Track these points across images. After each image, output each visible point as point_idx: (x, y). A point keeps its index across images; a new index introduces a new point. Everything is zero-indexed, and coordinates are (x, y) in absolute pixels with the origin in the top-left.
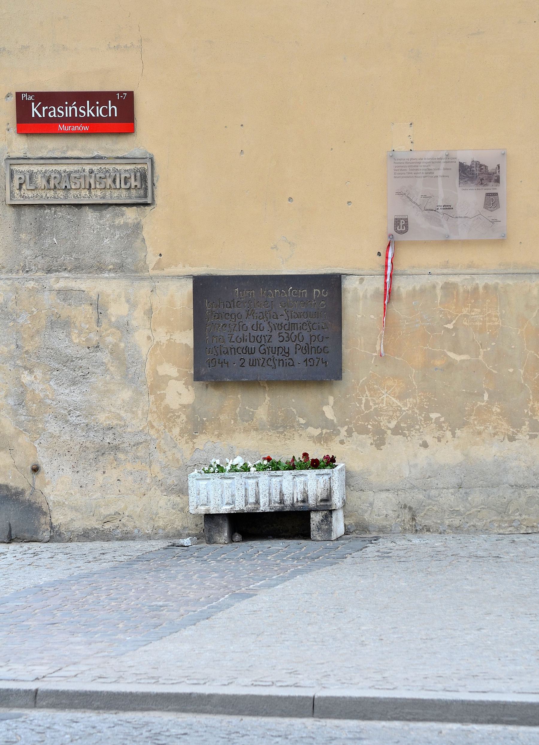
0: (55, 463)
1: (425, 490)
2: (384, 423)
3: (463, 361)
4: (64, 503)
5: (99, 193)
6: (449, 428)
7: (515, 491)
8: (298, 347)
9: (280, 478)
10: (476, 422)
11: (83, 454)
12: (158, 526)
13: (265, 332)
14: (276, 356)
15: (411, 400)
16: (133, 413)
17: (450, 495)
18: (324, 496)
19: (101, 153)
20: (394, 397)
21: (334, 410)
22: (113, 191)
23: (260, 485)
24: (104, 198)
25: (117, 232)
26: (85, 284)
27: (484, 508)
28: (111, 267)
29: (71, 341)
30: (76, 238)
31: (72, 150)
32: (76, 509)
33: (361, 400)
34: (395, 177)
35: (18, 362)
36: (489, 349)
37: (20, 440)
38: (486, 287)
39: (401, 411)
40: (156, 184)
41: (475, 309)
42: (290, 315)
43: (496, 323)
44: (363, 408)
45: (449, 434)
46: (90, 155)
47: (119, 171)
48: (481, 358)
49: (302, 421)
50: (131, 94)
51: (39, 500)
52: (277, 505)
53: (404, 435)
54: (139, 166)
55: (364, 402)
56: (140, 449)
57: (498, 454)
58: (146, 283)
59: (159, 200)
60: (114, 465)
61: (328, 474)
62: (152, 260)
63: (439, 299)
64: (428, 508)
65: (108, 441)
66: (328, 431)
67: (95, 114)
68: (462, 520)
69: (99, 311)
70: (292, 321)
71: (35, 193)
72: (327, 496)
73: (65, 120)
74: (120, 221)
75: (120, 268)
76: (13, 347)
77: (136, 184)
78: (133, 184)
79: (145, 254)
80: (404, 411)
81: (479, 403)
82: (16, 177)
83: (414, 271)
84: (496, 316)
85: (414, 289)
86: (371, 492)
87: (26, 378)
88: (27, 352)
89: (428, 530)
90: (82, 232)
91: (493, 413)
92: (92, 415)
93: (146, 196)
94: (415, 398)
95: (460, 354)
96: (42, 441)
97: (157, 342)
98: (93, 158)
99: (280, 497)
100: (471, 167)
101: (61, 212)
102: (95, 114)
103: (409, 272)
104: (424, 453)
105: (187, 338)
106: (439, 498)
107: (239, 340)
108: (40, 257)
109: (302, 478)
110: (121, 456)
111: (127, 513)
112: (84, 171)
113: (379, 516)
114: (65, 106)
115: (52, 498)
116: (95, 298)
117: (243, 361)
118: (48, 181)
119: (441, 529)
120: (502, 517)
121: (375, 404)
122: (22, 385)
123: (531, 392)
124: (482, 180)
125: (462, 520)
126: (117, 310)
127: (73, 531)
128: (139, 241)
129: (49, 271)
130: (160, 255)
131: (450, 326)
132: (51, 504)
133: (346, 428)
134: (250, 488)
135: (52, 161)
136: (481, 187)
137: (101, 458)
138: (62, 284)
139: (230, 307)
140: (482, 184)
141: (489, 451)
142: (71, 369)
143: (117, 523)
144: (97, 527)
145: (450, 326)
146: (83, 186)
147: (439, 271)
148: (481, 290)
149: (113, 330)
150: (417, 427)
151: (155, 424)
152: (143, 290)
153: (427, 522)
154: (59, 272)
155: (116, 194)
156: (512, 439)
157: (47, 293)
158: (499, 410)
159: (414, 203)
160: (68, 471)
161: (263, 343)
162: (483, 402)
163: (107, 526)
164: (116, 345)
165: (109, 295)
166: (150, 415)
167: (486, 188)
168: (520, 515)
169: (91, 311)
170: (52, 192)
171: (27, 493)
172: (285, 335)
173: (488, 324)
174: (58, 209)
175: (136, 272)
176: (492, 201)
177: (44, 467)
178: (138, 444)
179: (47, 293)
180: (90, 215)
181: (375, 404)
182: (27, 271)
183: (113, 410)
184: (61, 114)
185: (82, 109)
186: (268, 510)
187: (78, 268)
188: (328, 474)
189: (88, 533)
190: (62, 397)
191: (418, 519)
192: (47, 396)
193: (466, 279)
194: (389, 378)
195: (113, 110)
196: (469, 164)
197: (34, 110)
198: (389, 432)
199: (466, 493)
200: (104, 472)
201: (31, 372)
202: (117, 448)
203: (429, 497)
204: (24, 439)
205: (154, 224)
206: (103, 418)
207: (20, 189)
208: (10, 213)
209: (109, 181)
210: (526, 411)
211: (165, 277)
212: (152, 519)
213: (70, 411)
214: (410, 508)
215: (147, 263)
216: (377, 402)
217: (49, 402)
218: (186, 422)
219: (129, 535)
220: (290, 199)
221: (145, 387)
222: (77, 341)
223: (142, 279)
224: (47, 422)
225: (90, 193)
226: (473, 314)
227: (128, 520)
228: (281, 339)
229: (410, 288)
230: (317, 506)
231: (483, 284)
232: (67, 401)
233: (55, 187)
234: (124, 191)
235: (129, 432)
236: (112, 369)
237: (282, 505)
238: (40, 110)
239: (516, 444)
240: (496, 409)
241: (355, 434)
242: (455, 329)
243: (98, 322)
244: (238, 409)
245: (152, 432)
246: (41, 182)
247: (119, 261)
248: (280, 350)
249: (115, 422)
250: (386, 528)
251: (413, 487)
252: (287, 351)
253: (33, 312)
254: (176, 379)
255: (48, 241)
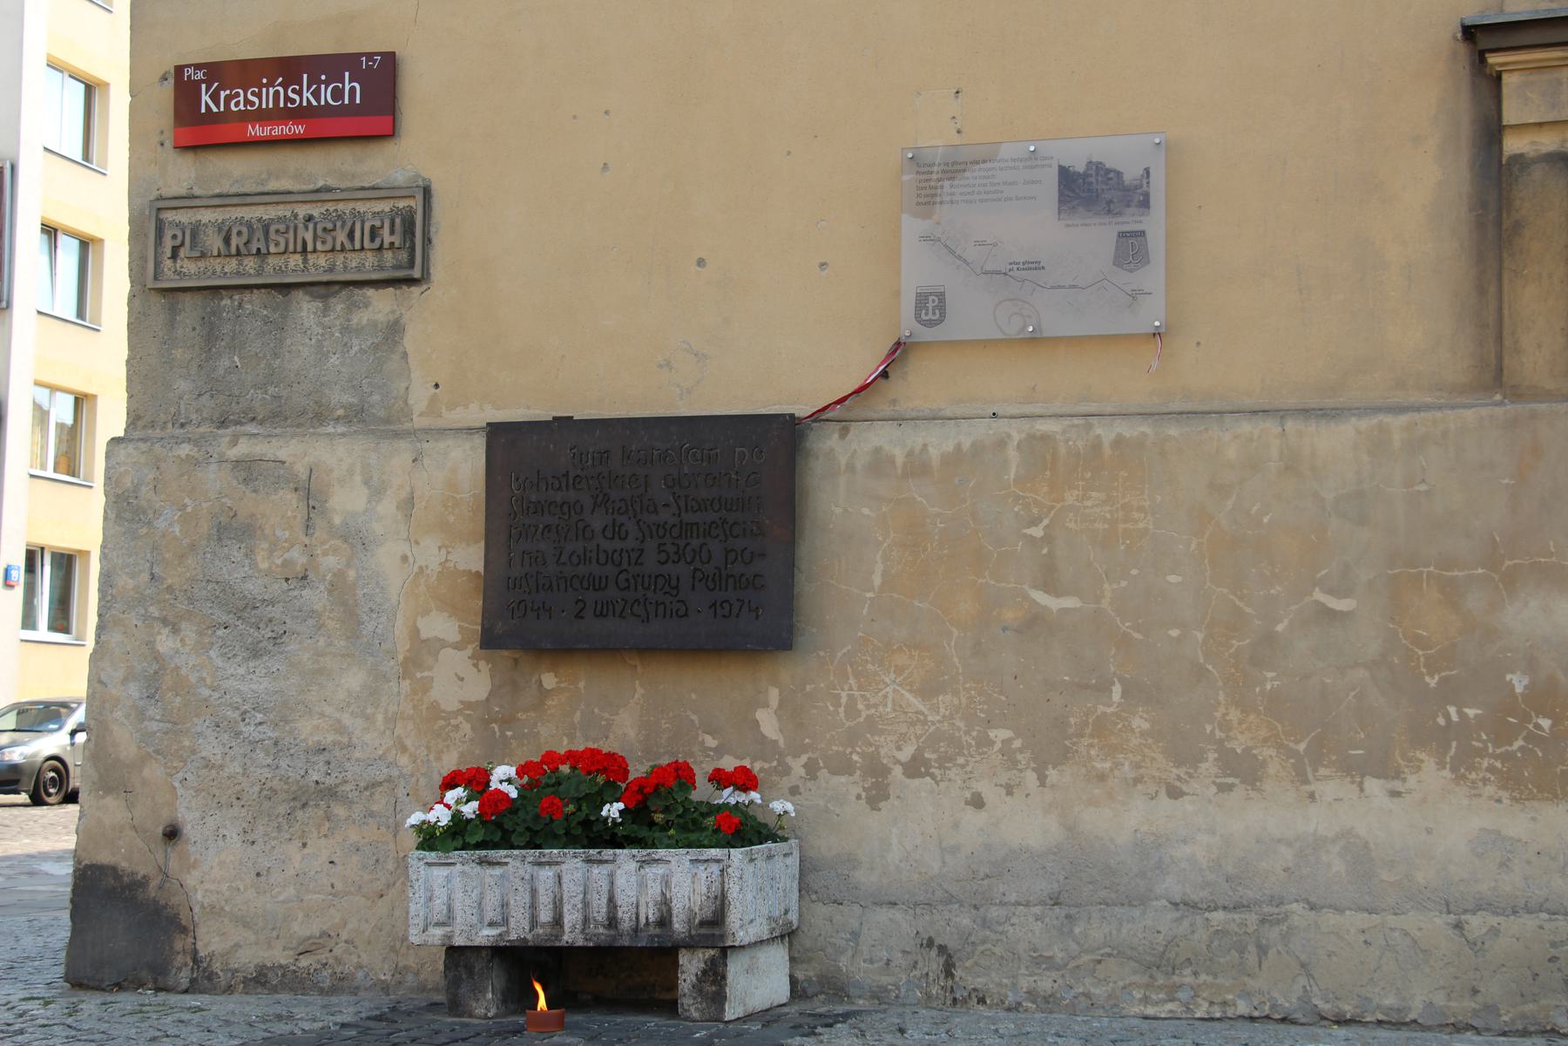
0: (210, 822)
1: (976, 907)
2: (887, 750)
3: (1065, 611)
4: (222, 909)
5: (322, 261)
6: (1033, 765)
7: (1182, 918)
8: (699, 575)
9: (609, 867)
10: (1093, 752)
11: (267, 804)
12: (405, 967)
13: (630, 543)
14: (650, 594)
15: (948, 697)
16: (367, 718)
17: (1031, 919)
18: (708, 913)
19: (331, 182)
20: (910, 691)
21: (780, 718)
22: (349, 255)
23: (565, 879)
24: (331, 270)
25: (355, 341)
26: (292, 450)
27: (1110, 955)
28: (340, 412)
29: (254, 565)
30: (276, 355)
31: (278, 178)
32: (244, 922)
33: (838, 697)
34: (918, 204)
35: (152, 609)
36: (1124, 584)
37: (146, 772)
38: (1119, 442)
39: (925, 722)
40: (435, 240)
41: (1094, 494)
42: (682, 504)
43: (1141, 525)
44: (842, 715)
45: (1031, 777)
46: (311, 187)
47: (356, 214)
48: (1105, 604)
49: (711, 742)
50: (390, 59)
51: (174, 900)
52: (601, 930)
53: (933, 777)
54: (401, 204)
55: (844, 701)
56: (377, 796)
57: (1144, 828)
58: (403, 444)
59: (437, 273)
60: (324, 830)
61: (718, 861)
62: (420, 396)
63: (1013, 470)
64: (981, 948)
65: (315, 778)
66: (766, 766)
67: (318, 100)
68: (1060, 981)
69: (311, 503)
70: (688, 517)
71: (202, 264)
72: (714, 912)
73: (262, 116)
74: (361, 317)
75: (357, 416)
76: (146, 577)
77: (393, 239)
78: (387, 239)
79: (404, 385)
80: (933, 723)
81: (1101, 708)
82: (168, 234)
83: (959, 411)
84: (1141, 509)
85: (958, 447)
86: (856, 908)
87: (165, 642)
88: (170, 589)
89: (982, 1001)
90: (288, 342)
91: (1132, 730)
92: (287, 722)
93: (411, 264)
94: (956, 693)
95: (1058, 595)
96: (189, 776)
97: (421, 568)
98: (317, 191)
99: (609, 912)
100: (1085, 175)
101: (253, 301)
102: (318, 100)
103: (948, 413)
104: (973, 820)
105: (471, 557)
106: (1007, 927)
107: (575, 559)
108: (207, 396)
109: (659, 870)
110: (340, 811)
111: (344, 936)
112: (296, 216)
113: (871, 961)
114: (261, 86)
115: (199, 896)
116: (305, 477)
117: (581, 605)
118: (227, 241)
119: (1011, 998)
120: (1151, 977)
121: (868, 707)
122: (157, 657)
123: (1220, 683)
124: (1110, 202)
125: (1060, 981)
126: (347, 501)
127: (237, 971)
128: (396, 357)
129: (223, 424)
130: (437, 386)
131: (1037, 532)
132: (196, 909)
133: (804, 758)
134: (541, 890)
135: (236, 200)
136: (1107, 219)
137: (299, 814)
138: (243, 449)
139: (560, 488)
140: (1109, 211)
141: (1123, 820)
142: (251, 625)
143: (323, 956)
144: (283, 962)
145: (1037, 532)
146: (291, 248)
147: (1014, 410)
148: (1107, 450)
149: (338, 542)
150: (961, 760)
151: (408, 743)
152: (399, 458)
153: (979, 982)
154: (241, 424)
155: (354, 260)
156: (1175, 793)
157: (213, 467)
158: (1146, 726)
159: (960, 257)
160: (233, 834)
161: (625, 566)
162: (1110, 706)
163: (304, 962)
164: (340, 574)
165: (331, 470)
166: (399, 725)
167: (1121, 219)
168: (1195, 974)
169: (294, 502)
170: (234, 262)
171: (154, 884)
172: (671, 549)
173: (1121, 526)
174: (247, 296)
175: (388, 421)
176: (1132, 249)
177: (187, 830)
178: (374, 785)
179: (213, 467)
180: (306, 308)
181: (868, 707)
182: (182, 425)
183: (328, 710)
184: (253, 104)
185: (294, 91)
186: (580, 943)
187: (277, 417)
188: (718, 861)
189: (265, 975)
190: (232, 684)
191: (958, 973)
192: (204, 679)
193: (1073, 426)
194: (900, 648)
195: (353, 90)
196: (1080, 167)
197: (205, 98)
198: (898, 771)
199: (1068, 917)
200: (304, 845)
201: (175, 630)
202: (331, 793)
203: (985, 923)
204: (154, 771)
205: (426, 319)
206: (308, 730)
207: (174, 256)
208: (158, 302)
209: (341, 237)
210: (1209, 728)
211: (442, 432)
212: (393, 949)
213: (245, 712)
214: (942, 949)
215: (411, 402)
216: (872, 701)
217: (206, 692)
218: (472, 740)
219: (346, 983)
220: (701, 262)
221: (392, 663)
222: (264, 565)
223: (397, 435)
224: (200, 734)
225: (305, 261)
226: (1089, 503)
227: (346, 951)
228: (663, 557)
229: (949, 446)
230: (691, 937)
231: (1113, 436)
232: (239, 692)
233: (238, 254)
234: (369, 254)
235: (358, 760)
236: (331, 624)
237: (612, 932)
238: (215, 98)
239: (1186, 804)
240: (1140, 723)
241: (823, 774)
242: (1048, 539)
243: (308, 527)
244: (578, 714)
245: (404, 760)
246: (214, 242)
247: (355, 401)
248: (661, 581)
249: (330, 738)
250: (886, 990)
251: (950, 899)
252: (674, 583)
253: (185, 506)
254: (457, 647)
255: (224, 363)
